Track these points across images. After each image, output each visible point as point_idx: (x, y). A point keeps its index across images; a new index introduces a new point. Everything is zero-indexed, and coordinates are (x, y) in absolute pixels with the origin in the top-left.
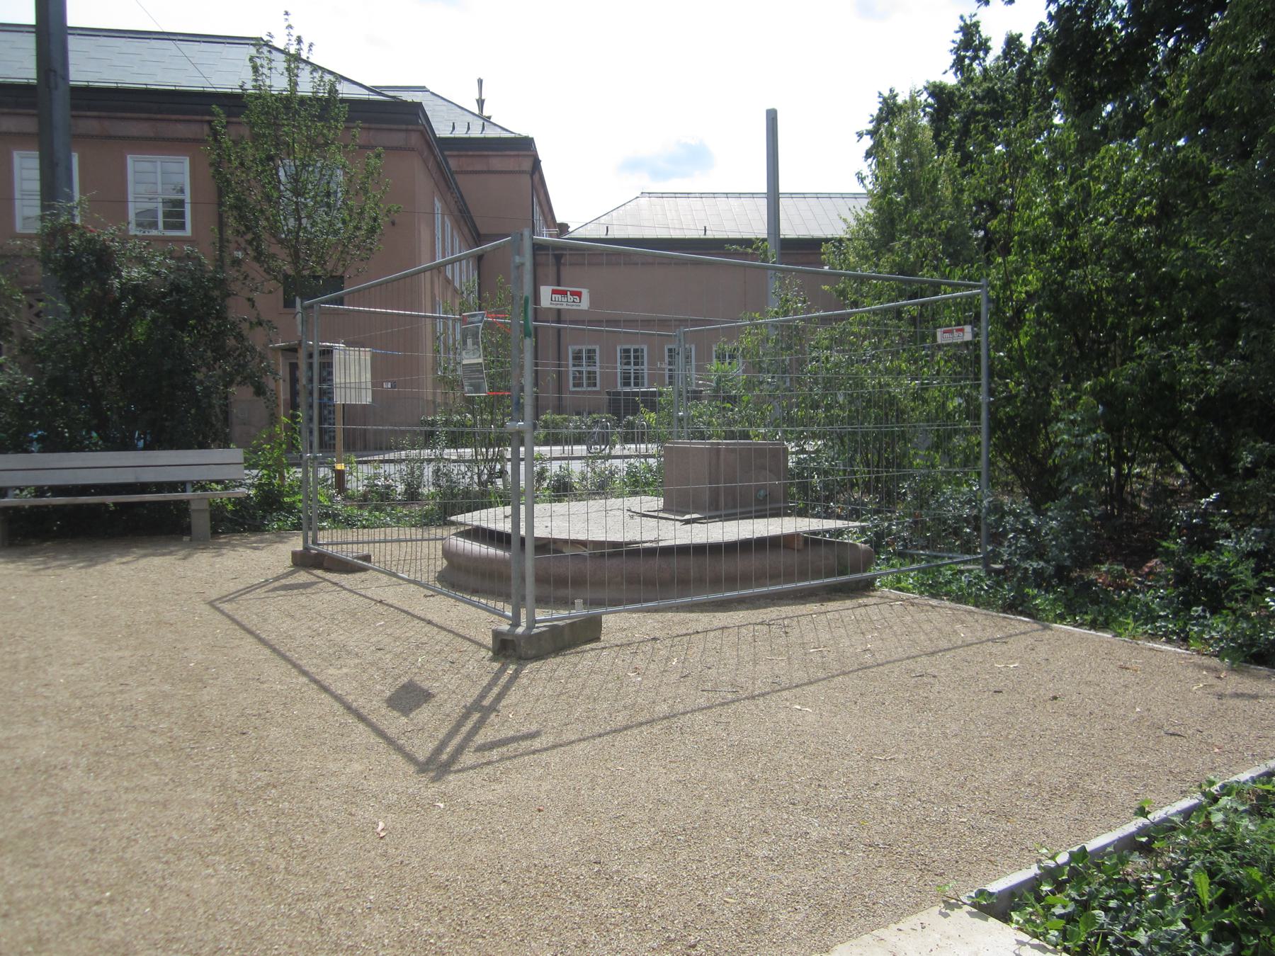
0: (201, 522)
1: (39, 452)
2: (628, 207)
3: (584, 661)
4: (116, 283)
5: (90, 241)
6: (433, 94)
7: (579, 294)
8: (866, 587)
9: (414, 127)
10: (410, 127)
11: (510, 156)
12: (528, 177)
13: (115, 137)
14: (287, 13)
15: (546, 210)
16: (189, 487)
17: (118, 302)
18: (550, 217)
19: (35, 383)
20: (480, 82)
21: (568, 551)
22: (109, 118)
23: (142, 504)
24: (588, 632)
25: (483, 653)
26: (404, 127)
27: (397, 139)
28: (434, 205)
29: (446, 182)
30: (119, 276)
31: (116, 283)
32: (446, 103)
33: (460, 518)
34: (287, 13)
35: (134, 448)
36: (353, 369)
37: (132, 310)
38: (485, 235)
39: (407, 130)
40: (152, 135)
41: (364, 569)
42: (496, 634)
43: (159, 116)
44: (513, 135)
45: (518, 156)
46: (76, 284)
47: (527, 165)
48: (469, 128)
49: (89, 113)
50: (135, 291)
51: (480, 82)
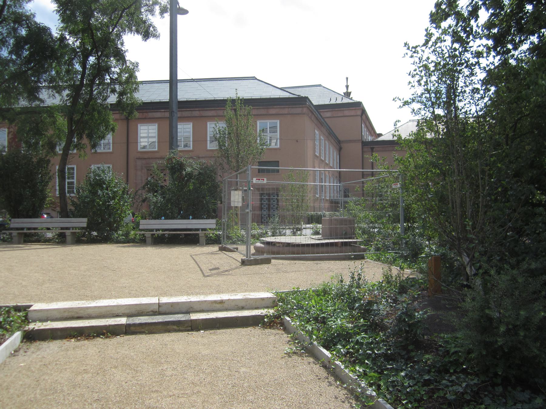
0: (202, 239)
1: (164, 219)
2: (403, 126)
3: (265, 267)
4: (184, 173)
5: (178, 161)
6: (324, 87)
7: (264, 180)
8: (362, 258)
9: (305, 106)
10: (303, 106)
11: (352, 109)
12: (360, 118)
13: (205, 116)
14: (236, 90)
15: (370, 129)
16: (200, 230)
17: (184, 178)
18: (372, 132)
19: (163, 201)
20: (347, 78)
21: (278, 245)
22: (202, 110)
23: (190, 234)
24: (267, 261)
25: (239, 263)
26: (301, 106)
27: (298, 110)
28: (315, 134)
29: (321, 123)
30: (185, 170)
31: (184, 173)
32: (328, 90)
33: (263, 239)
34: (236, 90)
35: (189, 219)
36: (237, 197)
37: (188, 180)
38: (342, 141)
39: (302, 107)
40: (216, 115)
41: (235, 251)
42: (242, 259)
43: (218, 108)
44: (353, 101)
45: (355, 109)
46: (175, 173)
47: (359, 113)
48: (336, 100)
49: (196, 109)
50: (190, 175)
51: (347, 78)
